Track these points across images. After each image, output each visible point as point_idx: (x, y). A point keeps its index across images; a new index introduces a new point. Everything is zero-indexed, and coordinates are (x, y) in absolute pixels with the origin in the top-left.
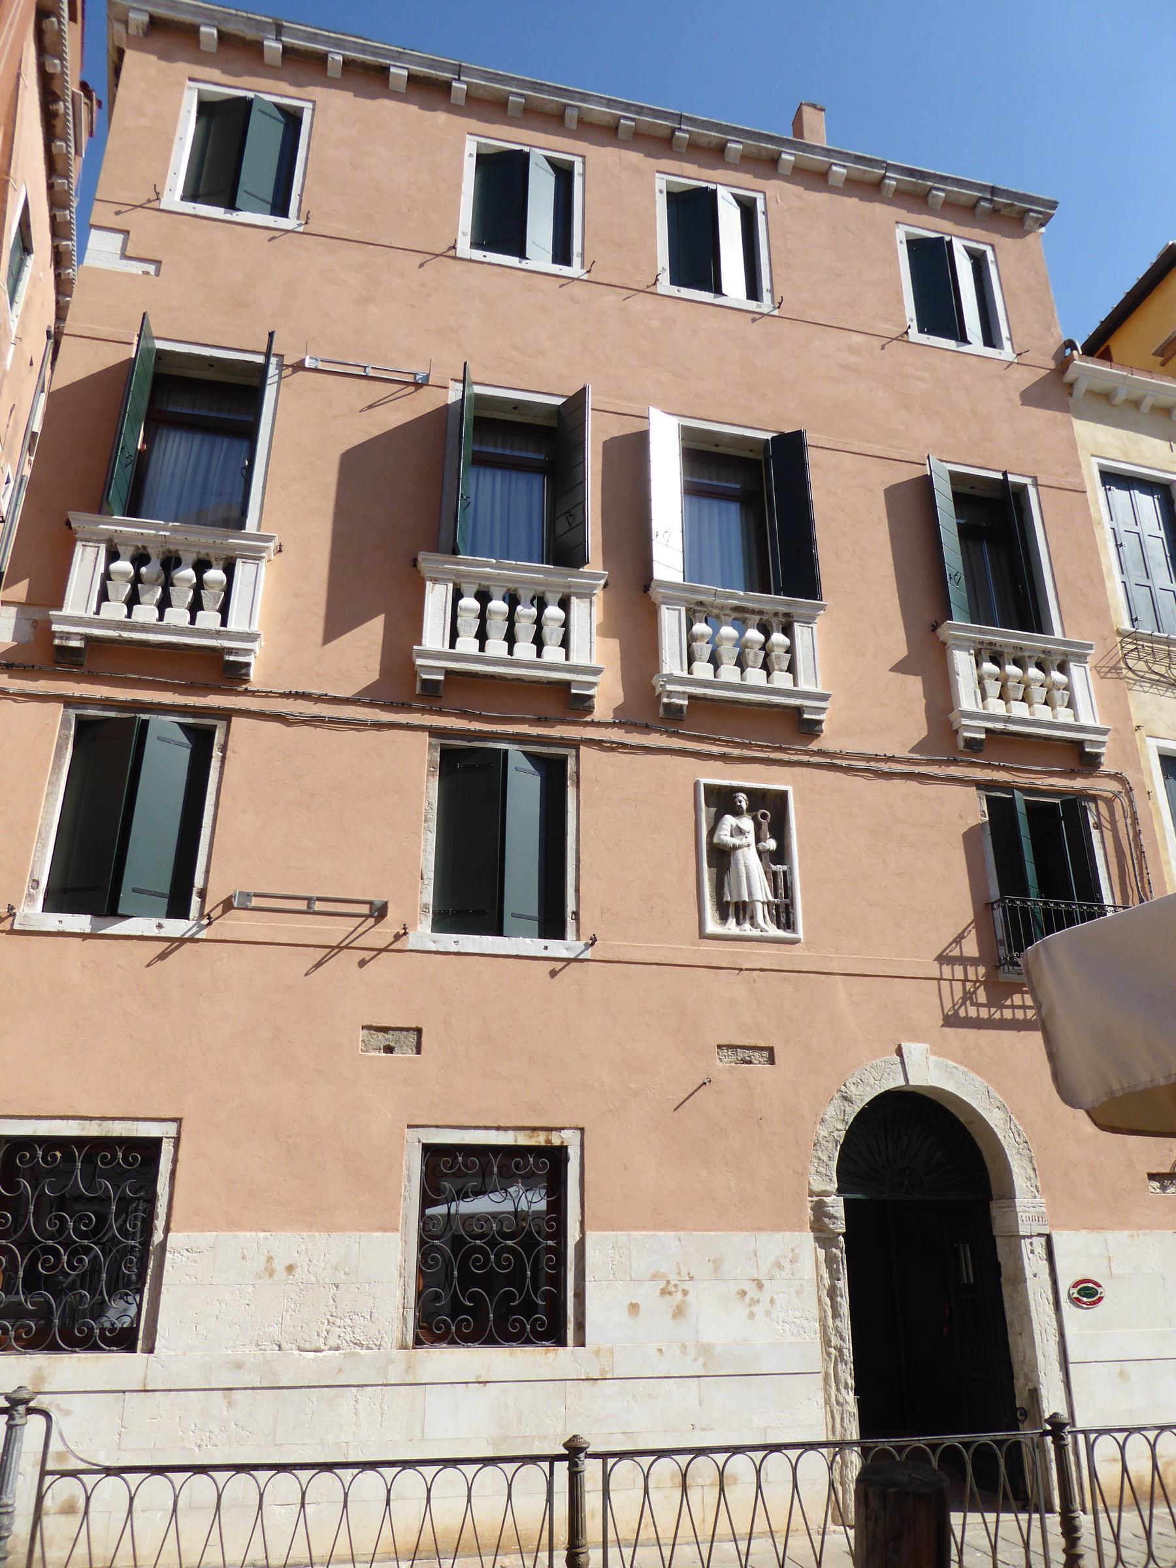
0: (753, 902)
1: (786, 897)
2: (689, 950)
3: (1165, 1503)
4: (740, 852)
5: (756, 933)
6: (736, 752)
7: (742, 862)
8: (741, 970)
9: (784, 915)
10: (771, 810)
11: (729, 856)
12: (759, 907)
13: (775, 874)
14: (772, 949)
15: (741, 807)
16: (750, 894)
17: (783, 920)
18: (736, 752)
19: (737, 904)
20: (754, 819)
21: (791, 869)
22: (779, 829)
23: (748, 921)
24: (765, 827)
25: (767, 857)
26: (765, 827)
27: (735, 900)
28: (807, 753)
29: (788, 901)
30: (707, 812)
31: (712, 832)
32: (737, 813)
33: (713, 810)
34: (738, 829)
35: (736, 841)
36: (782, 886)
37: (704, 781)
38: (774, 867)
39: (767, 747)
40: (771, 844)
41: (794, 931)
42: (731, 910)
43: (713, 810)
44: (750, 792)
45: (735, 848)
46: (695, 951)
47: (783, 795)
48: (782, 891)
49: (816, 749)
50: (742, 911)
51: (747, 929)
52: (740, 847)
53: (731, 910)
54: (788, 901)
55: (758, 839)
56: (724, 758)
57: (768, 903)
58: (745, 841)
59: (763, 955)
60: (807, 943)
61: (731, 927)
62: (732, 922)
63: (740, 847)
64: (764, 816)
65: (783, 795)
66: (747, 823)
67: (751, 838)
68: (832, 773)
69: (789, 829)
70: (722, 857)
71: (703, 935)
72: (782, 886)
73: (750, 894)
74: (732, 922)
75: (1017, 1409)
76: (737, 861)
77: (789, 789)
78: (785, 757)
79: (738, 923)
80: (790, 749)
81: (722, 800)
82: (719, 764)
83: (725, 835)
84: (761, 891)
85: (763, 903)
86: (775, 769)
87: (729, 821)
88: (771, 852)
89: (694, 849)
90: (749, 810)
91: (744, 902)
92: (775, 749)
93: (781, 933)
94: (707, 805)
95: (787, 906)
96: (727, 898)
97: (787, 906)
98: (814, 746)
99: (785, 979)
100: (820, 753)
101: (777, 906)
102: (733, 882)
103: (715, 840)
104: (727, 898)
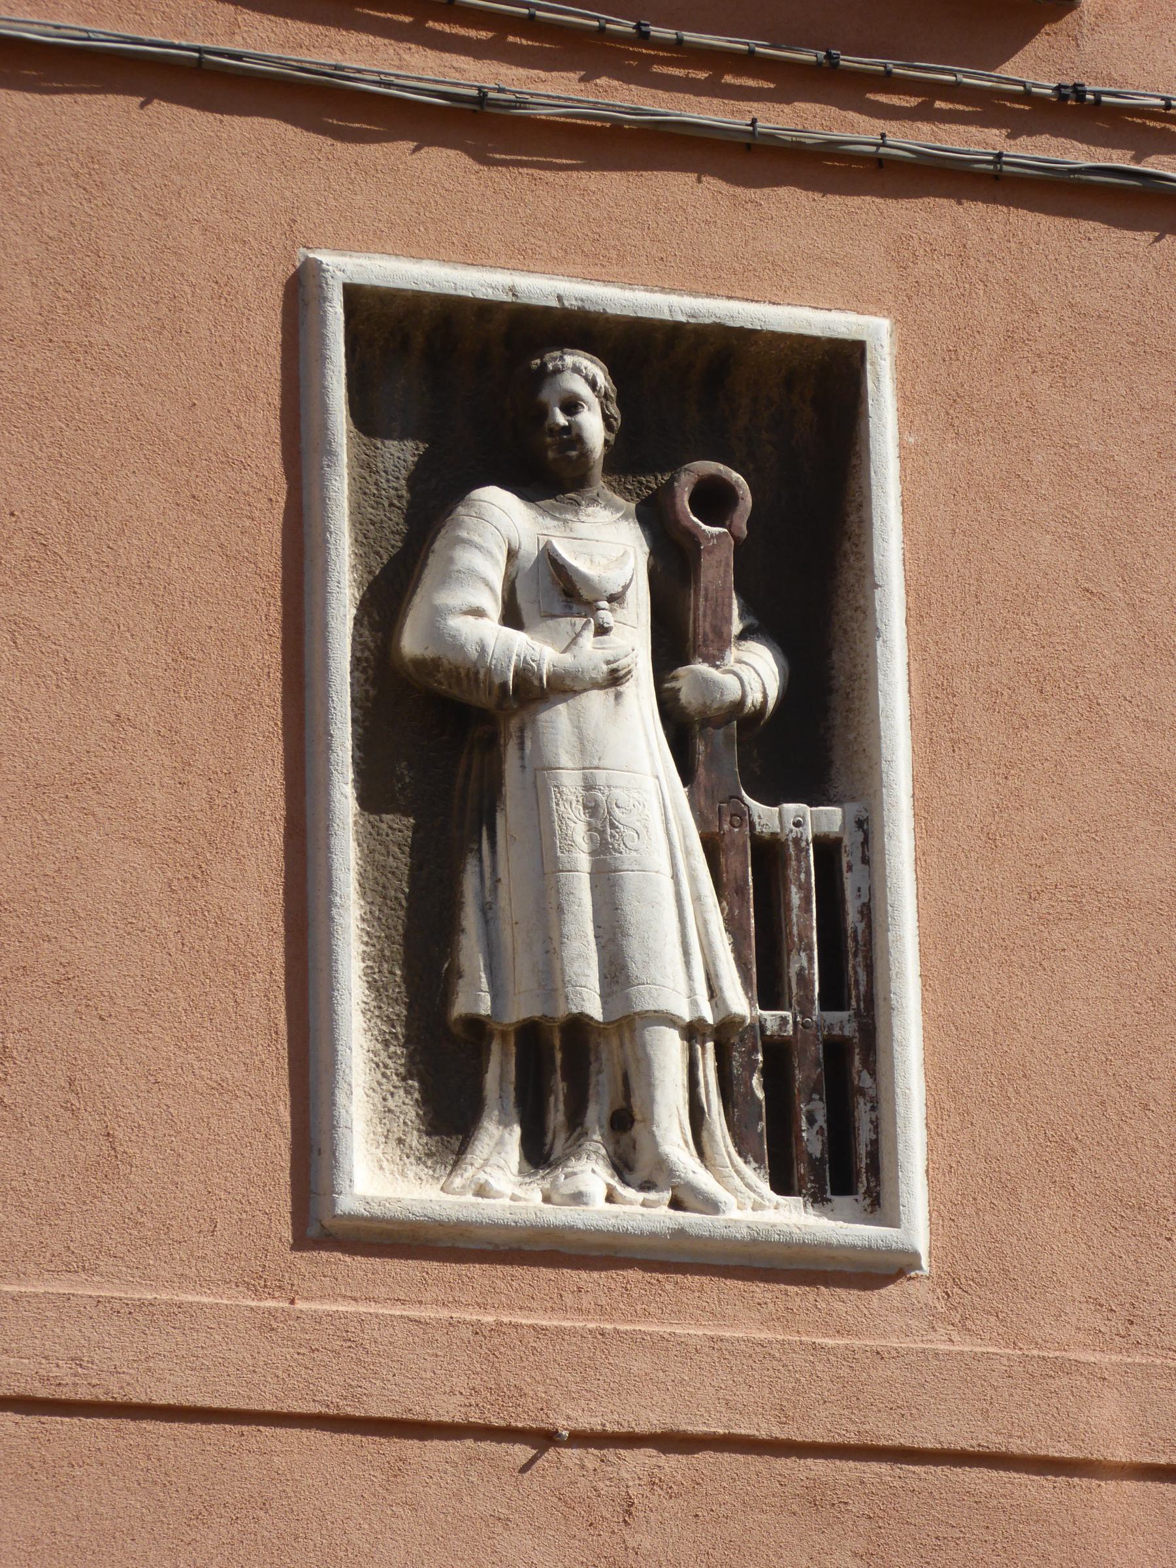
0: (630, 1024)
1: (833, 997)
2: (223, 1316)
3: (482, 586)
4: (559, 719)
5: (643, 1213)
6: (553, 90)
7: (570, 781)
8: (544, 1439)
9: (812, 1103)
10: (755, 463)
11: (492, 747)
12: (669, 1053)
13: (769, 854)
14: (743, 1318)
15: (573, 438)
16: (616, 973)
17: (811, 1139)
18: (553, 90)
19: (530, 1036)
20: (655, 518)
21: (867, 828)
22: (806, 581)
23: (596, 1142)
24: (717, 569)
25: (720, 751)
26: (717, 569)
27: (520, 1010)
28: (991, 107)
29: (842, 1022)
30: (364, 468)
31: (390, 592)
32: (550, 477)
33: (400, 454)
34: (555, 577)
35: (537, 649)
36: (807, 921)
37: (345, 267)
38: (766, 816)
39: (747, 62)
40: (753, 672)
41: (878, 1203)
42: (498, 1074)
43: (400, 454)
44: (631, 348)
45: (534, 692)
46: (267, 1324)
47: (836, 370)
48: (805, 963)
49: (1045, 84)
50: (565, 1078)
51: (592, 1191)
52: (563, 687)
53: (498, 1074)
54: (842, 1022)
55: (673, 643)
56: (478, 126)
57: (724, 1035)
58: (591, 653)
59: (685, 1350)
60: (951, 1281)
61: (497, 1181)
62: (498, 1147)
63: (563, 687)
64: (713, 500)
65: (836, 370)
66: (608, 544)
67: (631, 636)
68: (1139, 241)
69: (866, 615)
70: (450, 751)
71: (317, 1224)
72: (807, 921)
73: (616, 973)
74: (498, 1147)
75: (542, 358)
76: (541, 776)
77: (877, 331)
78: (857, 129)
79: (538, 1155)
80: (887, 82)
81: (458, 395)
82: (444, 164)
83: (470, 615)
84: (684, 957)
85: (693, 1032)
86: (790, 206)
87: (501, 522)
88: (743, 720)
89: (272, 691)
90: (625, 459)
91: (578, 1025)
92: (794, 82)
93: (793, 1218)
94: (365, 418)
95: (836, 1053)
96: (476, 998)
97: (836, 1053)
98: (1035, 67)
99: (815, 1499)
100: (1073, 109)
101: (778, 1054)
102: (512, 903)
103: (412, 642)
104: (476, 998)
